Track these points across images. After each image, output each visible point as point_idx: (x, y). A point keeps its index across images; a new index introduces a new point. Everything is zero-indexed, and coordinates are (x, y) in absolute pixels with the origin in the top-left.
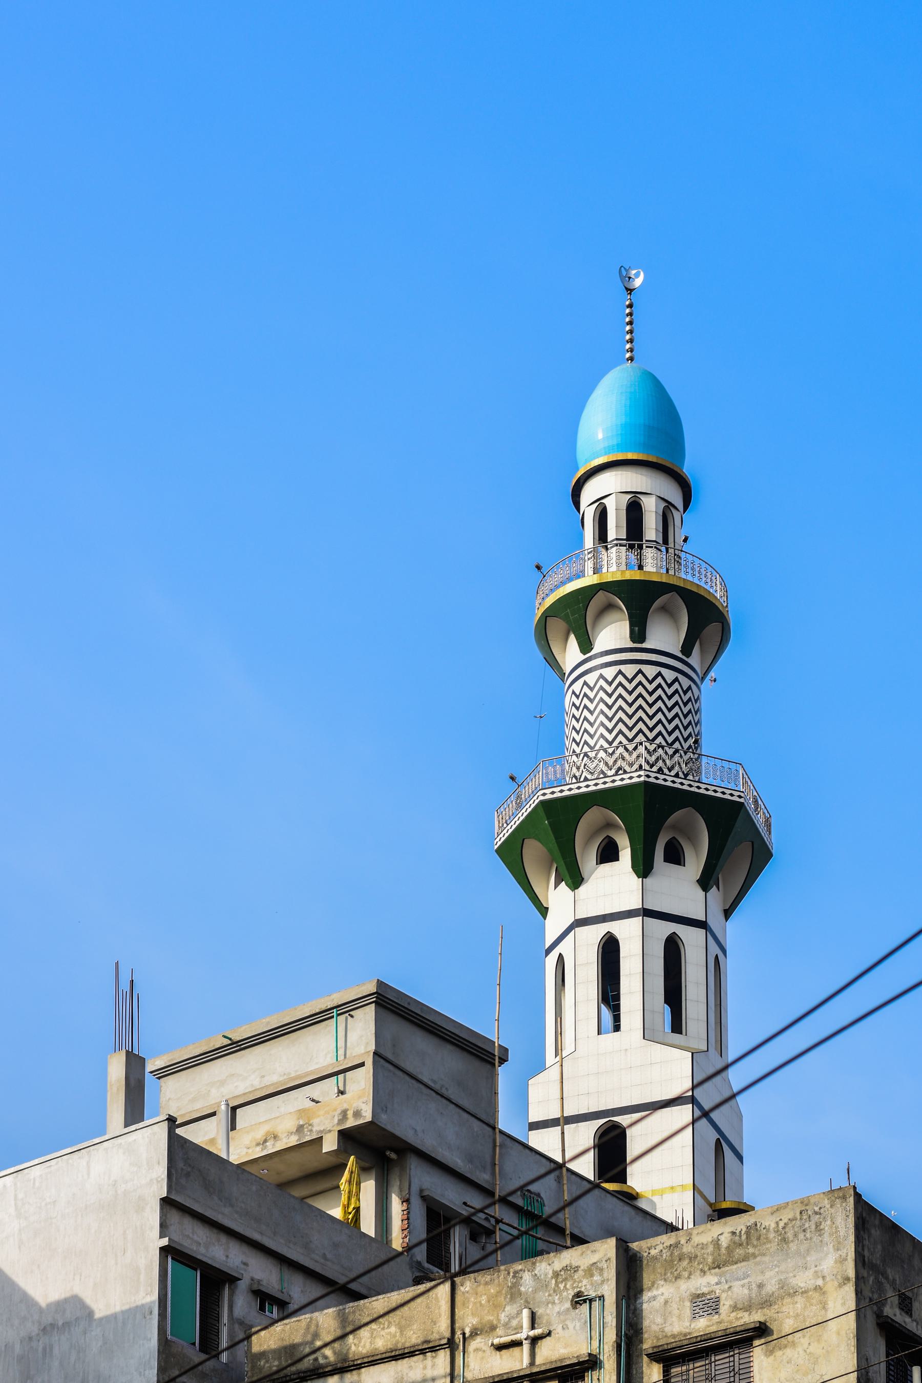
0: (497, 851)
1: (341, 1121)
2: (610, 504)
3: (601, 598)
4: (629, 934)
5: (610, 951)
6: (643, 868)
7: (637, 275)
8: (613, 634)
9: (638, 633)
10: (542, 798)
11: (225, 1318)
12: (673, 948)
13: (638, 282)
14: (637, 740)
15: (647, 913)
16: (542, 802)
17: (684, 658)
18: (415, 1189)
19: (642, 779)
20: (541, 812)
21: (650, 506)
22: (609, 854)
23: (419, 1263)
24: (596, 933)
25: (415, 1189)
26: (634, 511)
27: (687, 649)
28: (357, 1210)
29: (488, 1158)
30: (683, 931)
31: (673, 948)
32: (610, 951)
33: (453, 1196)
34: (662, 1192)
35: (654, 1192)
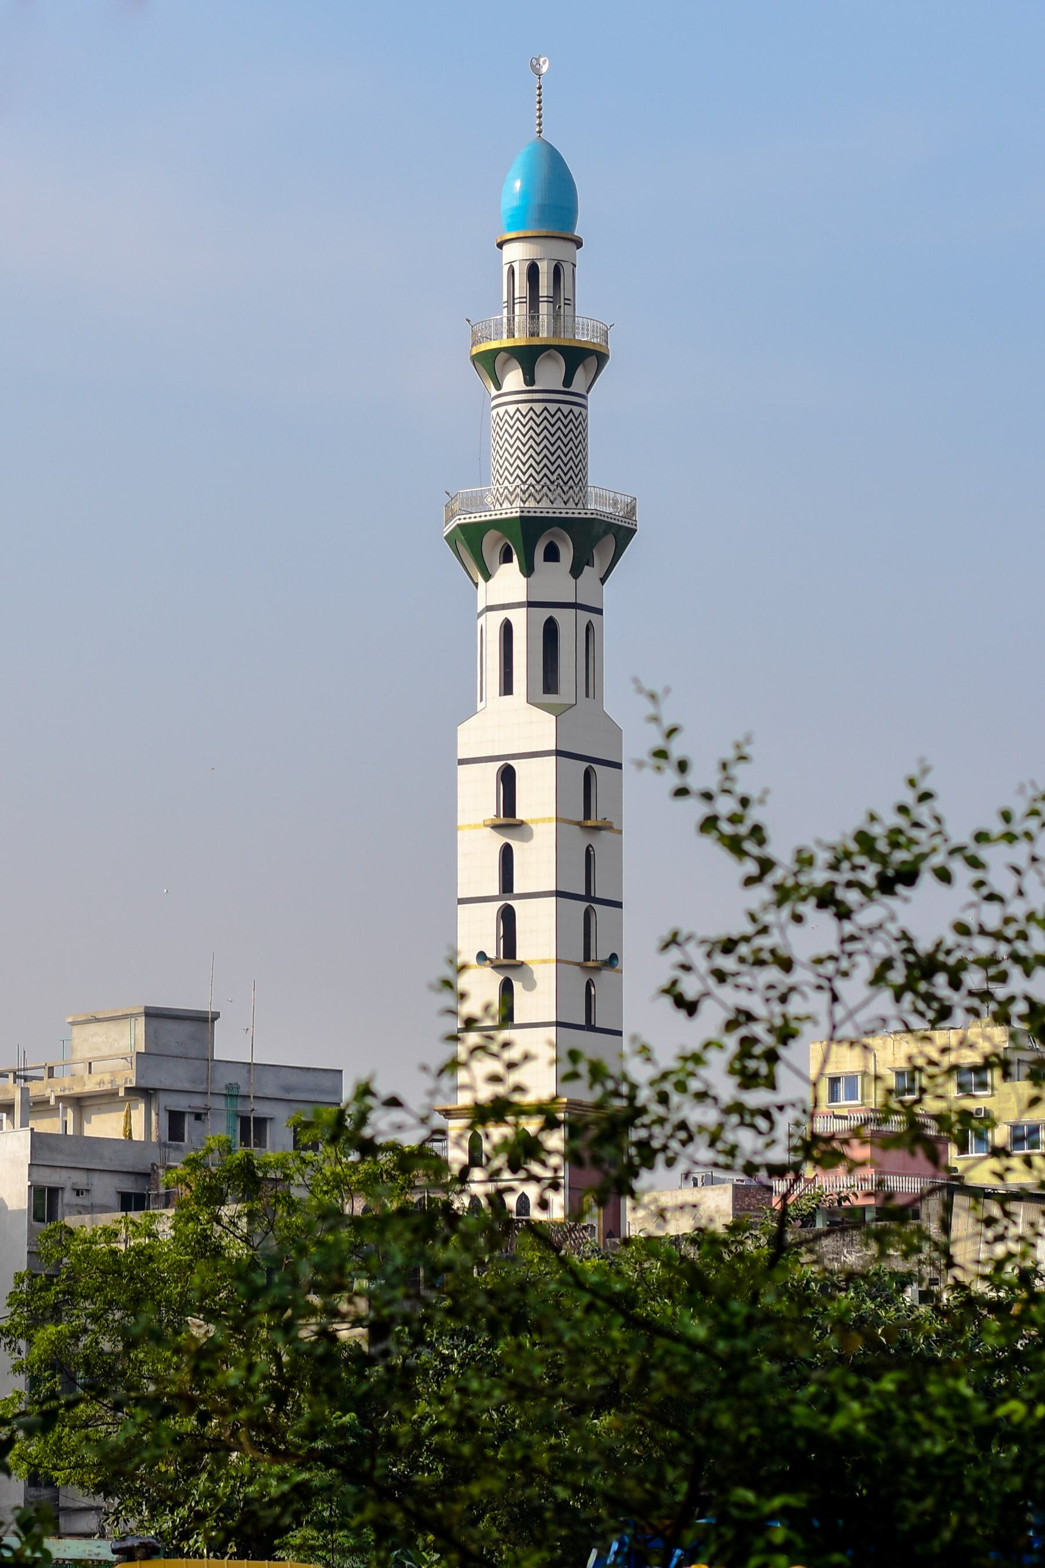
0: (446, 538)
1: (126, 1083)
2: (516, 266)
3: (503, 356)
4: (519, 619)
5: (507, 628)
6: (528, 569)
7: (544, 62)
8: (514, 379)
9: (530, 378)
10: (458, 522)
11: (60, 1205)
12: (551, 631)
13: (545, 69)
14: (516, 484)
15: (530, 604)
16: (459, 525)
17: (566, 389)
18: (162, 1107)
19: (518, 514)
20: (458, 530)
21: (544, 268)
22: (507, 558)
23: (165, 1143)
24: (499, 617)
25: (162, 1107)
26: (533, 272)
27: (568, 381)
28: (130, 1130)
29: (205, 1077)
30: (556, 613)
31: (551, 631)
32: (507, 628)
33: (181, 1103)
34: (537, 821)
35: (533, 821)
